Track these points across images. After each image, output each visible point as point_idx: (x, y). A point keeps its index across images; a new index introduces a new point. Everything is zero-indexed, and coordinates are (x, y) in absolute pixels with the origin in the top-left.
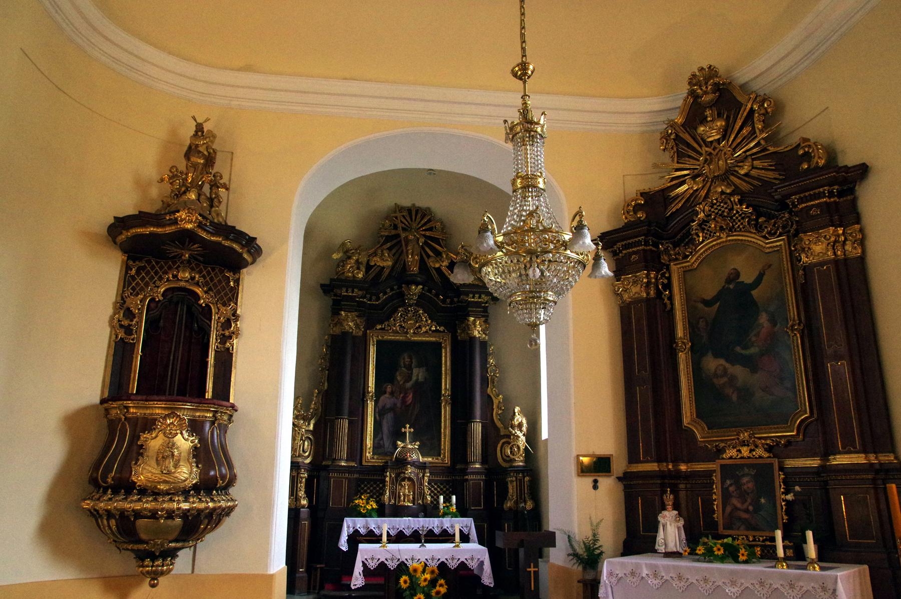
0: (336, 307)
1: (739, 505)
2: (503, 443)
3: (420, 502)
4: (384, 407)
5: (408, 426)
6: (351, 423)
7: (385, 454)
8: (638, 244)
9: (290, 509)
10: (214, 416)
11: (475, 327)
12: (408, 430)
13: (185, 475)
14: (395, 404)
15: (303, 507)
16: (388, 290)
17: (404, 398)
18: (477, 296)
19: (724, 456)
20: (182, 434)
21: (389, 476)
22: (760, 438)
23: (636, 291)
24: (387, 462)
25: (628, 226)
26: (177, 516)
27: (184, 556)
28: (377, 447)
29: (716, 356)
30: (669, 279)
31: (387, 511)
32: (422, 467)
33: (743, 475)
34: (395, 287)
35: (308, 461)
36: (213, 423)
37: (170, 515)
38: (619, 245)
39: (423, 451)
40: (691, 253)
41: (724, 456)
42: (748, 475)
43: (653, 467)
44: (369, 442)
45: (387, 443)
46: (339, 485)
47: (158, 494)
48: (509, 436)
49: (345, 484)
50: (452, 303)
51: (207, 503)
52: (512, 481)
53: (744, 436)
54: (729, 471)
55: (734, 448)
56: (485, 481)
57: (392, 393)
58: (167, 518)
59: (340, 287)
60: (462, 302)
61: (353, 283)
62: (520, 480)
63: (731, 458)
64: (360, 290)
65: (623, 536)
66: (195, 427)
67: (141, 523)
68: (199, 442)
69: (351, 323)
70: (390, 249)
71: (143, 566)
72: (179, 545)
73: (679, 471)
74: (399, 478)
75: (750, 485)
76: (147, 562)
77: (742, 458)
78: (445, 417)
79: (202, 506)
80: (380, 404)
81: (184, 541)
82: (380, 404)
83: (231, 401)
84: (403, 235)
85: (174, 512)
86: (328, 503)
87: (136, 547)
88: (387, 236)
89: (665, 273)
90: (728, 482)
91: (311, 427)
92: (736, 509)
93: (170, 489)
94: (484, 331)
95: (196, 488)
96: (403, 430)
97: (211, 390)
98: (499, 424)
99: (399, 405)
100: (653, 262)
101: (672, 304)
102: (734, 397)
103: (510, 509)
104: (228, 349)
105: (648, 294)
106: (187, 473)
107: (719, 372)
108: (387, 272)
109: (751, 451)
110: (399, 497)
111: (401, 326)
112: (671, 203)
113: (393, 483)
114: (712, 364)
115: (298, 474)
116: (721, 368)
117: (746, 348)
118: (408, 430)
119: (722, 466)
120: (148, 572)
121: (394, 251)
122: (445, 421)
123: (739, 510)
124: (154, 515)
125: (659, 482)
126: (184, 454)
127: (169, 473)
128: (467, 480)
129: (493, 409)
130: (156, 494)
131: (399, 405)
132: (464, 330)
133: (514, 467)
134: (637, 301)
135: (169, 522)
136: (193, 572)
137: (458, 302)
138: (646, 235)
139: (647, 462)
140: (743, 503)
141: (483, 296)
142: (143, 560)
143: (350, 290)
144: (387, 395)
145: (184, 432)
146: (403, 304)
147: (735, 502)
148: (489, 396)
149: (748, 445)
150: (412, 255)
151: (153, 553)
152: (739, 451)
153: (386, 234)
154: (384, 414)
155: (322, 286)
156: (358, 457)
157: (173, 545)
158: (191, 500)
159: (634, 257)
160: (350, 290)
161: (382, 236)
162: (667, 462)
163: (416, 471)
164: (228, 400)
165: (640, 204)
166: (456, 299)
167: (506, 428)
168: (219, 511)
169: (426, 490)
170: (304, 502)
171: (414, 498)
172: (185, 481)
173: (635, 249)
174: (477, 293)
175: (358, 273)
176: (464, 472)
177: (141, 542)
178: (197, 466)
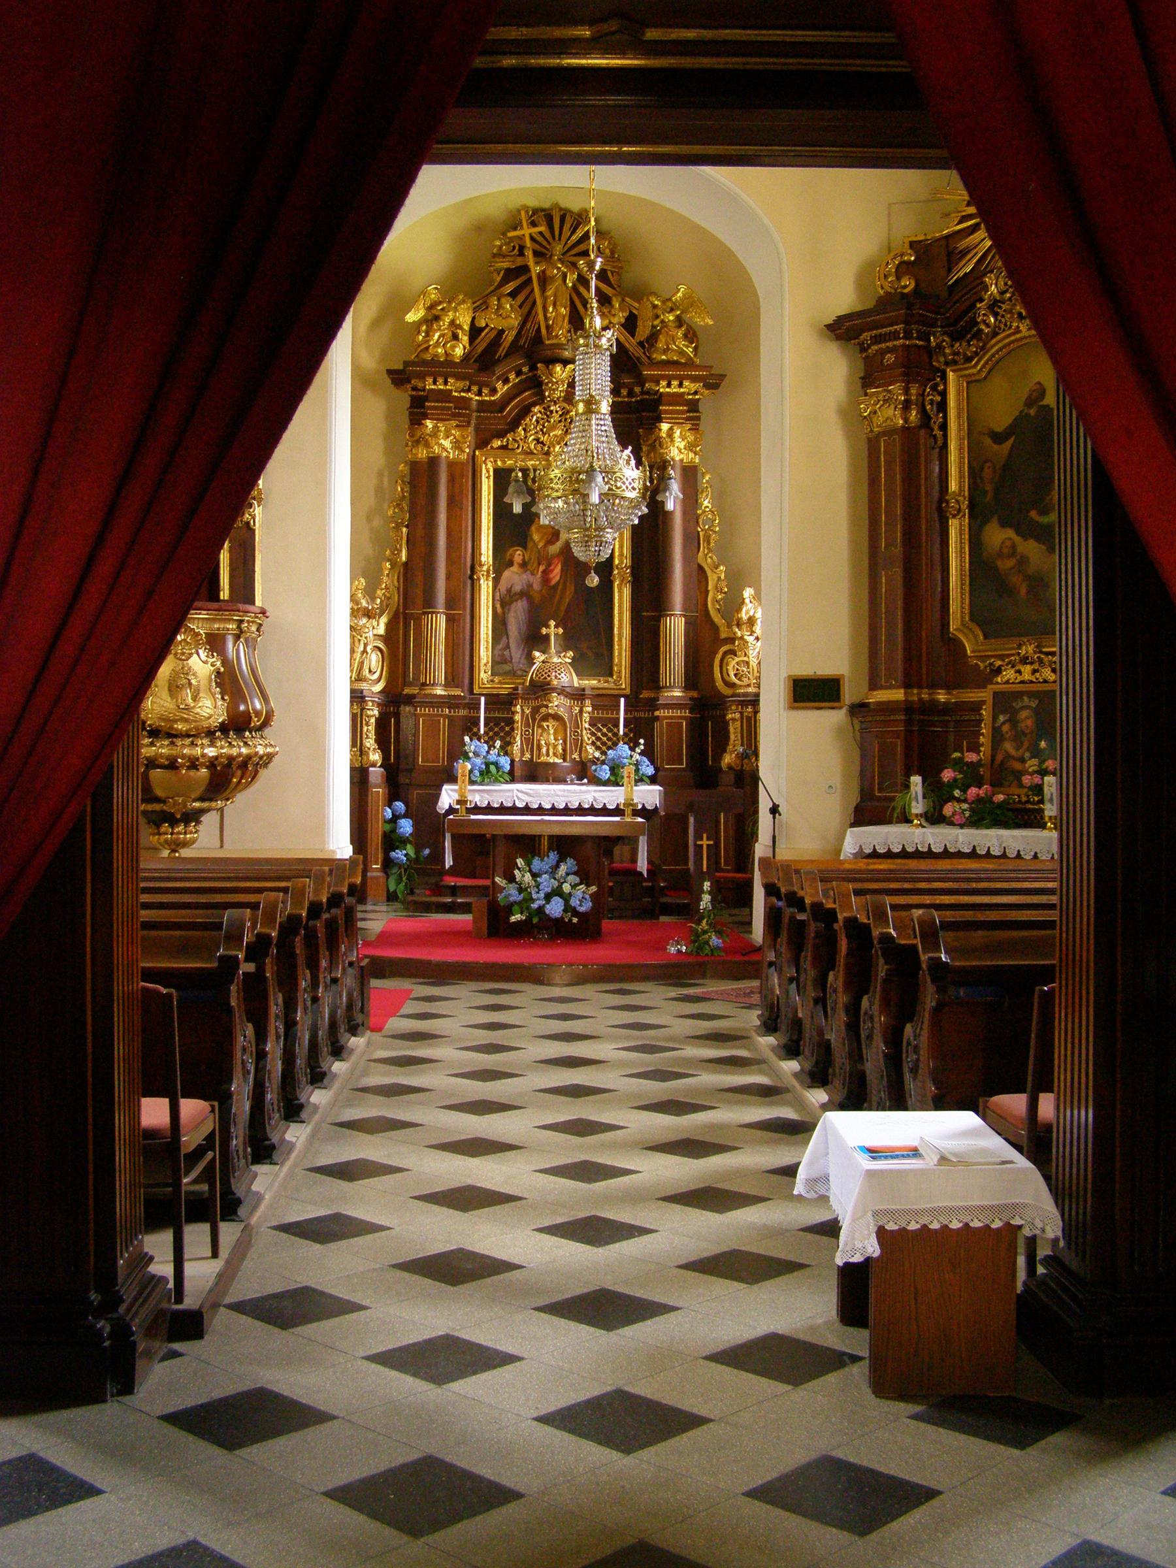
0: (418, 409)
1: (1013, 752)
2: (725, 654)
3: (576, 756)
4: (509, 591)
5: (552, 623)
6: (450, 620)
7: (512, 674)
8: (894, 336)
9: (352, 769)
10: (239, 627)
11: (672, 441)
12: (552, 630)
13: (209, 711)
14: (530, 586)
15: (374, 765)
16: (512, 376)
17: (545, 573)
18: (675, 383)
19: (999, 680)
20: (198, 654)
21: (520, 711)
22: (1048, 654)
23: (891, 416)
24: (516, 689)
25: (885, 302)
26: (203, 765)
27: (209, 821)
28: (499, 662)
29: (1004, 524)
30: (944, 394)
31: (518, 773)
32: (578, 696)
33: (1022, 708)
34: (525, 369)
35: (378, 688)
36: (237, 637)
37: (193, 764)
38: (866, 335)
39: (578, 665)
40: (976, 353)
41: (999, 680)
42: (1027, 707)
43: (898, 695)
44: (484, 653)
45: (516, 653)
46: (432, 725)
47: (175, 736)
48: (732, 640)
49: (444, 724)
50: (631, 394)
51: (240, 747)
52: (734, 720)
53: (1028, 649)
54: (1003, 702)
55: (1013, 667)
56: (691, 722)
57: (524, 565)
58: (189, 768)
59: (422, 377)
60: (648, 393)
61: (445, 369)
62: (749, 719)
63: (1007, 682)
64: (457, 379)
65: (855, 798)
66: (215, 643)
67: (156, 774)
68: (223, 664)
69: (446, 442)
70: (513, 295)
71: (159, 834)
72: (206, 805)
73: (934, 702)
74: (538, 717)
75: (1029, 722)
76: (165, 827)
77: (1022, 682)
78: (620, 607)
79: (234, 752)
80: (503, 585)
81: (211, 800)
82: (503, 585)
83: (258, 603)
84: (536, 270)
85: (198, 759)
86: (415, 759)
87: (150, 807)
88: (508, 271)
89: (937, 385)
90: (1002, 718)
91: (381, 630)
92: (1008, 756)
93: (190, 729)
94: (690, 447)
95: (224, 728)
96: (561, 631)
97: (227, 587)
98: (717, 619)
99: (536, 587)
100: (921, 370)
101: (945, 436)
102: (1023, 591)
103: (730, 767)
104: (248, 523)
105: (906, 420)
106: (211, 708)
107: (1005, 551)
108: (509, 337)
109: (1034, 671)
110: (539, 748)
111: (538, 441)
112: (960, 259)
113: (527, 725)
114: (997, 536)
115: (362, 710)
116: (1008, 543)
117: (1044, 512)
118: (552, 630)
119: (996, 694)
120: (166, 841)
121: (520, 298)
122: (621, 613)
123: (1013, 758)
124: (172, 765)
125: (903, 717)
126: (204, 683)
127: (188, 709)
128: (657, 718)
129: (707, 592)
130: (172, 736)
131: (536, 587)
132: (653, 447)
133: (738, 695)
134: (889, 432)
135: (192, 773)
136: (222, 847)
137: (643, 393)
138: (906, 323)
139: (890, 687)
140: (1017, 750)
141: (686, 383)
142: (158, 826)
143: (440, 380)
144: (515, 569)
145: (201, 652)
146: (541, 400)
147: (1008, 746)
148: (701, 569)
149: (1031, 663)
150: (554, 305)
151: (173, 814)
152: (1019, 672)
153: (506, 265)
154: (510, 603)
155: (390, 372)
156: (466, 681)
157: (197, 805)
158: (219, 744)
159: (890, 358)
160: (440, 380)
161: (498, 271)
162: (920, 687)
163: (568, 702)
164: (254, 604)
165: (909, 263)
166: (637, 390)
167: (729, 626)
168: (256, 759)
169: (586, 736)
170: (376, 757)
171: (564, 750)
172: (209, 718)
173: (889, 344)
174: (675, 377)
175: (453, 347)
176: (653, 704)
177: (157, 800)
178: (223, 698)
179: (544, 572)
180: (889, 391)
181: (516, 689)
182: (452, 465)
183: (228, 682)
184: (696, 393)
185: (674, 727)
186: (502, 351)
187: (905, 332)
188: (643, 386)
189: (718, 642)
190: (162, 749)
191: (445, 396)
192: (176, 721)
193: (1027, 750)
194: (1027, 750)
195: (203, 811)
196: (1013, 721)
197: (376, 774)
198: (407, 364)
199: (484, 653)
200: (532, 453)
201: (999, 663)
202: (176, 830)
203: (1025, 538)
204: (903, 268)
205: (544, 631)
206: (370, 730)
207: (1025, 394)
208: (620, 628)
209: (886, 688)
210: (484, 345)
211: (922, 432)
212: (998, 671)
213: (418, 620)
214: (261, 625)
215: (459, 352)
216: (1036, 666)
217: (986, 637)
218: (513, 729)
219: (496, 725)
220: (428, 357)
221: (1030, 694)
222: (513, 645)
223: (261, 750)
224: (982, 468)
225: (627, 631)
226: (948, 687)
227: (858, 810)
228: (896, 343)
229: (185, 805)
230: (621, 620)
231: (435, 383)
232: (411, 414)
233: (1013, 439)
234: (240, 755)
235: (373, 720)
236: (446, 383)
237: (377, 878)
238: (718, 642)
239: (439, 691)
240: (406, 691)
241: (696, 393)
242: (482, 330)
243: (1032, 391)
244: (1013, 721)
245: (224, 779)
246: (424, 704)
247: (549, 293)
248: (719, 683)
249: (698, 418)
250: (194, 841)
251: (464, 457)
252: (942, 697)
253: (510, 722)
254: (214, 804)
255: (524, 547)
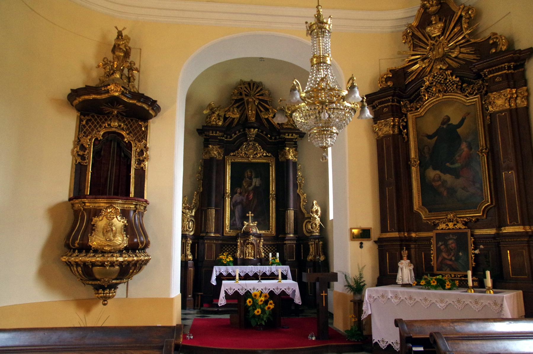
0: (206, 143)
1: (446, 257)
2: (307, 222)
3: (258, 257)
4: (236, 202)
5: (250, 212)
6: (216, 211)
7: (237, 229)
8: (388, 101)
10: (135, 207)
11: (290, 153)
12: (250, 215)
14: (242, 200)
15: (190, 260)
16: (237, 132)
19: (438, 228)
20: (117, 217)
21: (239, 241)
22: (460, 218)
23: (387, 130)
24: (238, 234)
25: (382, 90)
26: (116, 265)
28: (232, 226)
29: (435, 169)
32: (259, 236)
33: (449, 239)
34: (241, 130)
35: (192, 233)
36: (135, 211)
37: (112, 264)
38: (376, 102)
39: (259, 227)
40: (420, 106)
41: (438, 228)
42: (451, 239)
43: (396, 235)
44: (227, 222)
45: (238, 222)
46: (210, 247)
47: (105, 253)
49: (214, 247)
50: (275, 139)
51: (133, 257)
52: (312, 244)
54: (441, 237)
55: (444, 223)
56: (296, 245)
57: (240, 193)
58: (110, 266)
59: (208, 131)
60: (281, 139)
61: (216, 128)
62: (317, 244)
63: (442, 229)
64: (220, 132)
66: (125, 213)
67: (96, 269)
68: (127, 222)
69: (215, 152)
70: (238, 107)
71: (98, 294)
72: (118, 281)
74: (245, 243)
75: (453, 245)
76: (101, 291)
77: (449, 229)
79: (131, 259)
80: (234, 200)
81: (121, 279)
82: (234, 200)
83: (145, 198)
84: (246, 99)
85: (114, 263)
88: (236, 100)
90: (440, 243)
91: (193, 214)
92: (444, 259)
93: (111, 250)
94: (295, 156)
95: (127, 249)
98: (304, 211)
99: (245, 200)
100: (397, 112)
101: (408, 138)
102: (445, 193)
103: (311, 260)
104: (142, 168)
105: (394, 132)
108: (236, 121)
109: (454, 225)
110: (246, 254)
111: (245, 153)
112: (409, 75)
114: (432, 173)
115: (186, 241)
117: (452, 163)
118: (250, 215)
120: (101, 297)
121: (240, 108)
124: (103, 264)
126: (119, 230)
127: (110, 240)
129: (300, 202)
130: (103, 252)
131: (245, 200)
132: (283, 155)
133: (313, 236)
134: (386, 136)
135: (112, 268)
136: (127, 297)
137: (279, 138)
138: (393, 96)
139: (392, 232)
142: (98, 290)
143: (214, 132)
144: (238, 194)
145: (118, 217)
146: (246, 140)
147: (444, 255)
148: (298, 195)
149: (453, 222)
150: (251, 110)
152: (447, 225)
153: (235, 98)
155: (198, 130)
156: (221, 232)
158: (124, 256)
160: (214, 132)
161: (233, 100)
162: (404, 232)
163: (255, 239)
165: (390, 77)
166: (278, 137)
167: (308, 213)
169: (261, 250)
170: (190, 257)
171: (254, 254)
173: (386, 105)
176: (284, 239)
177: (96, 280)
178: (127, 236)
179: (247, 196)
180: (386, 121)
181: (238, 234)
182: (218, 161)
183: (131, 229)
184: (296, 139)
185: (291, 246)
186: (234, 125)
187: (392, 100)
188: (279, 136)
189: (304, 218)
190: (99, 258)
191: (216, 137)
192: (105, 246)
193: (453, 256)
194: (453, 256)
195: (118, 284)
196: (446, 245)
197: (190, 263)
198: (203, 126)
199: (227, 222)
200: (243, 157)
201: (437, 221)
202: (106, 292)
203: (445, 173)
204: (388, 79)
205: (247, 215)
206: (189, 248)
207: (440, 121)
208: (272, 214)
209: (390, 232)
210: (228, 123)
211: (399, 136)
212: (437, 225)
213: (206, 212)
214: (145, 207)
215: (220, 124)
216: (455, 223)
217: (429, 212)
218: (237, 248)
219: (228, 246)
220: (210, 125)
221: (454, 234)
222: (237, 220)
223: (142, 258)
224: (424, 149)
225: (274, 215)
226: (415, 232)
227: (379, 279)
228: (389, 104)
229: (109, 282)
230: (272, 212)
231: (212, 133)
232: (204, 144)
233: (436, 137)
234: (133, 260)
235: (190, 245)
236: (216, 133)
237: (190, 300)
238: (304, 218)
239: (212, 235)
240: (201, 235)
241: (296, 139)
242: (228, 118)
243: (444, 119)
244: (446, 245)
245: (126, 271)
246: (206, 239)
247: (249, 106)
248: (305, 232)
249: (297, 147)
250: (113, 296)
251: (221, 158)
252: (413, 235)
253: (236, 245)
254: (122, 281)
255: (241, 187)
